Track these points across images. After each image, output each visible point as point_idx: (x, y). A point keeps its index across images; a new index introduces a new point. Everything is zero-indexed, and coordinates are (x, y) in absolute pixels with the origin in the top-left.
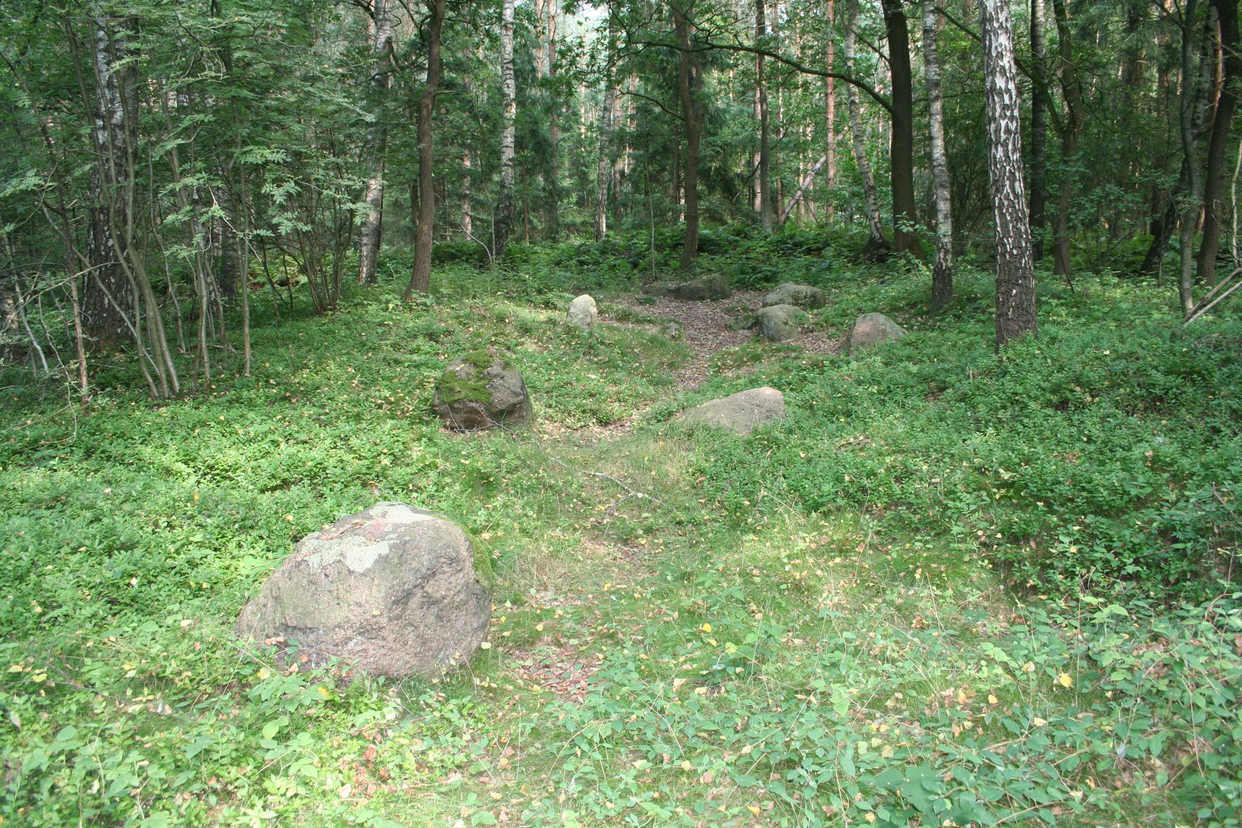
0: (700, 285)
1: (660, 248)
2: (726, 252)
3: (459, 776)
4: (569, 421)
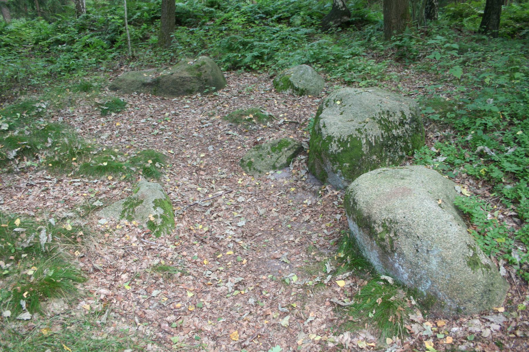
0: (186, 74)
1: (136, 23)
2: (204, 23)
3: (336, 124)
4: (369, 68)
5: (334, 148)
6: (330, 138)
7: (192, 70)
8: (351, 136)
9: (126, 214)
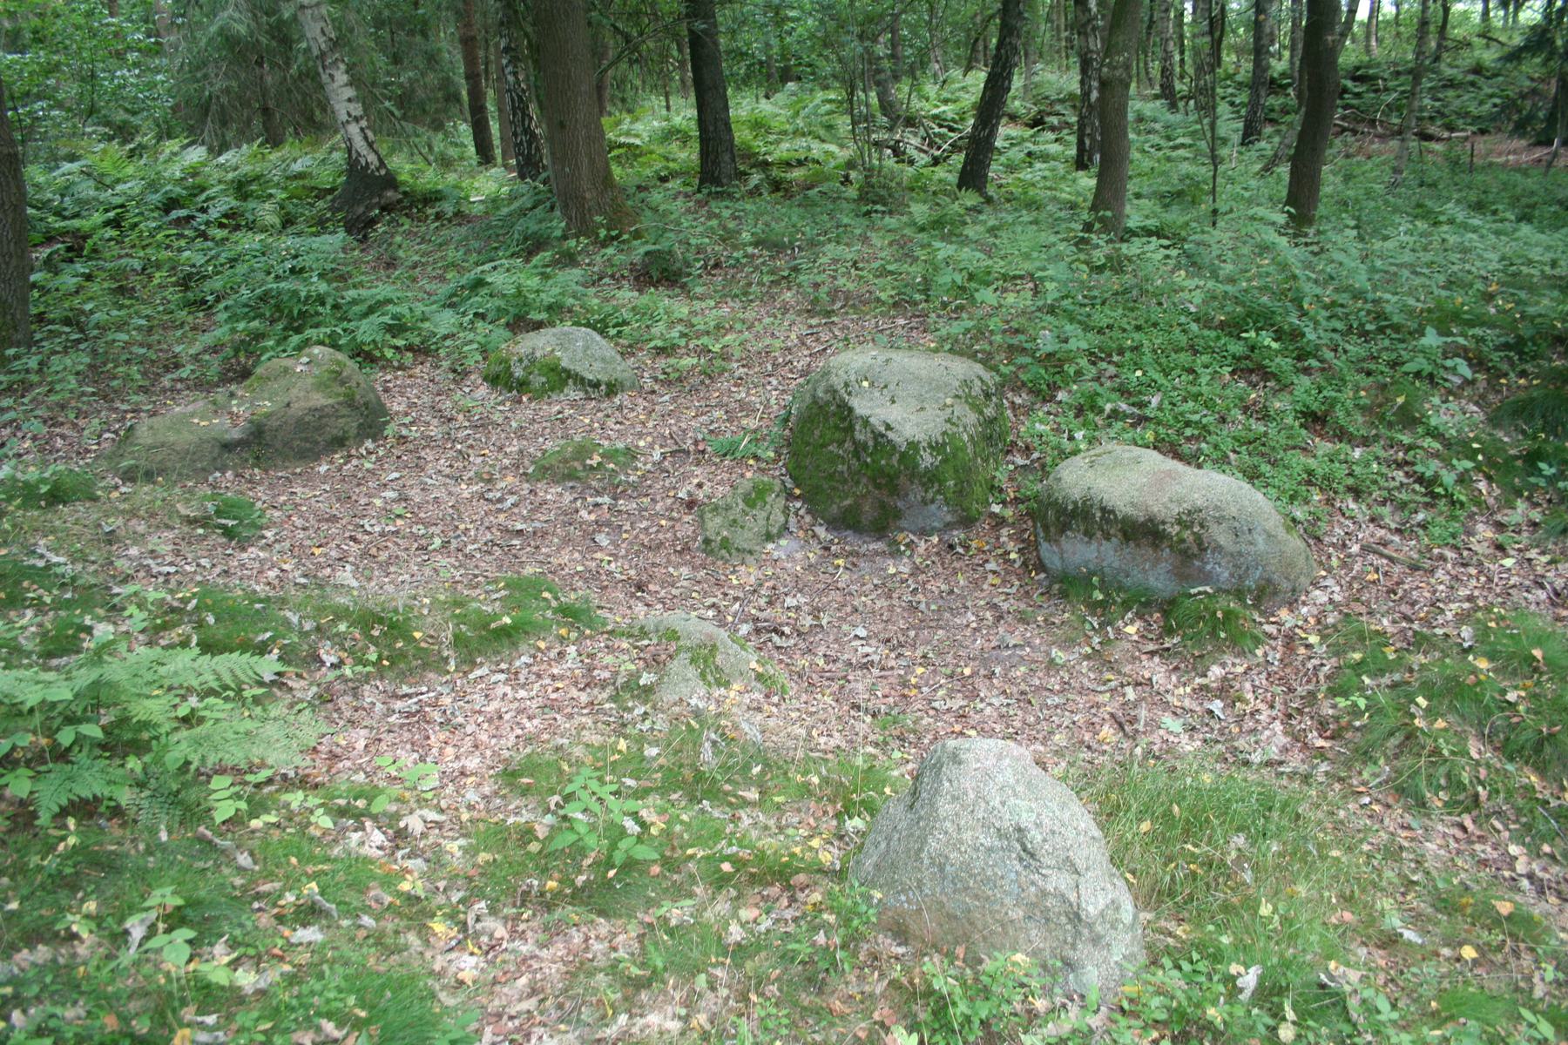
5: (927, 460)
6: (913, 445)
7: (327, 387)
8: (944, 433)
9: (709, 678)
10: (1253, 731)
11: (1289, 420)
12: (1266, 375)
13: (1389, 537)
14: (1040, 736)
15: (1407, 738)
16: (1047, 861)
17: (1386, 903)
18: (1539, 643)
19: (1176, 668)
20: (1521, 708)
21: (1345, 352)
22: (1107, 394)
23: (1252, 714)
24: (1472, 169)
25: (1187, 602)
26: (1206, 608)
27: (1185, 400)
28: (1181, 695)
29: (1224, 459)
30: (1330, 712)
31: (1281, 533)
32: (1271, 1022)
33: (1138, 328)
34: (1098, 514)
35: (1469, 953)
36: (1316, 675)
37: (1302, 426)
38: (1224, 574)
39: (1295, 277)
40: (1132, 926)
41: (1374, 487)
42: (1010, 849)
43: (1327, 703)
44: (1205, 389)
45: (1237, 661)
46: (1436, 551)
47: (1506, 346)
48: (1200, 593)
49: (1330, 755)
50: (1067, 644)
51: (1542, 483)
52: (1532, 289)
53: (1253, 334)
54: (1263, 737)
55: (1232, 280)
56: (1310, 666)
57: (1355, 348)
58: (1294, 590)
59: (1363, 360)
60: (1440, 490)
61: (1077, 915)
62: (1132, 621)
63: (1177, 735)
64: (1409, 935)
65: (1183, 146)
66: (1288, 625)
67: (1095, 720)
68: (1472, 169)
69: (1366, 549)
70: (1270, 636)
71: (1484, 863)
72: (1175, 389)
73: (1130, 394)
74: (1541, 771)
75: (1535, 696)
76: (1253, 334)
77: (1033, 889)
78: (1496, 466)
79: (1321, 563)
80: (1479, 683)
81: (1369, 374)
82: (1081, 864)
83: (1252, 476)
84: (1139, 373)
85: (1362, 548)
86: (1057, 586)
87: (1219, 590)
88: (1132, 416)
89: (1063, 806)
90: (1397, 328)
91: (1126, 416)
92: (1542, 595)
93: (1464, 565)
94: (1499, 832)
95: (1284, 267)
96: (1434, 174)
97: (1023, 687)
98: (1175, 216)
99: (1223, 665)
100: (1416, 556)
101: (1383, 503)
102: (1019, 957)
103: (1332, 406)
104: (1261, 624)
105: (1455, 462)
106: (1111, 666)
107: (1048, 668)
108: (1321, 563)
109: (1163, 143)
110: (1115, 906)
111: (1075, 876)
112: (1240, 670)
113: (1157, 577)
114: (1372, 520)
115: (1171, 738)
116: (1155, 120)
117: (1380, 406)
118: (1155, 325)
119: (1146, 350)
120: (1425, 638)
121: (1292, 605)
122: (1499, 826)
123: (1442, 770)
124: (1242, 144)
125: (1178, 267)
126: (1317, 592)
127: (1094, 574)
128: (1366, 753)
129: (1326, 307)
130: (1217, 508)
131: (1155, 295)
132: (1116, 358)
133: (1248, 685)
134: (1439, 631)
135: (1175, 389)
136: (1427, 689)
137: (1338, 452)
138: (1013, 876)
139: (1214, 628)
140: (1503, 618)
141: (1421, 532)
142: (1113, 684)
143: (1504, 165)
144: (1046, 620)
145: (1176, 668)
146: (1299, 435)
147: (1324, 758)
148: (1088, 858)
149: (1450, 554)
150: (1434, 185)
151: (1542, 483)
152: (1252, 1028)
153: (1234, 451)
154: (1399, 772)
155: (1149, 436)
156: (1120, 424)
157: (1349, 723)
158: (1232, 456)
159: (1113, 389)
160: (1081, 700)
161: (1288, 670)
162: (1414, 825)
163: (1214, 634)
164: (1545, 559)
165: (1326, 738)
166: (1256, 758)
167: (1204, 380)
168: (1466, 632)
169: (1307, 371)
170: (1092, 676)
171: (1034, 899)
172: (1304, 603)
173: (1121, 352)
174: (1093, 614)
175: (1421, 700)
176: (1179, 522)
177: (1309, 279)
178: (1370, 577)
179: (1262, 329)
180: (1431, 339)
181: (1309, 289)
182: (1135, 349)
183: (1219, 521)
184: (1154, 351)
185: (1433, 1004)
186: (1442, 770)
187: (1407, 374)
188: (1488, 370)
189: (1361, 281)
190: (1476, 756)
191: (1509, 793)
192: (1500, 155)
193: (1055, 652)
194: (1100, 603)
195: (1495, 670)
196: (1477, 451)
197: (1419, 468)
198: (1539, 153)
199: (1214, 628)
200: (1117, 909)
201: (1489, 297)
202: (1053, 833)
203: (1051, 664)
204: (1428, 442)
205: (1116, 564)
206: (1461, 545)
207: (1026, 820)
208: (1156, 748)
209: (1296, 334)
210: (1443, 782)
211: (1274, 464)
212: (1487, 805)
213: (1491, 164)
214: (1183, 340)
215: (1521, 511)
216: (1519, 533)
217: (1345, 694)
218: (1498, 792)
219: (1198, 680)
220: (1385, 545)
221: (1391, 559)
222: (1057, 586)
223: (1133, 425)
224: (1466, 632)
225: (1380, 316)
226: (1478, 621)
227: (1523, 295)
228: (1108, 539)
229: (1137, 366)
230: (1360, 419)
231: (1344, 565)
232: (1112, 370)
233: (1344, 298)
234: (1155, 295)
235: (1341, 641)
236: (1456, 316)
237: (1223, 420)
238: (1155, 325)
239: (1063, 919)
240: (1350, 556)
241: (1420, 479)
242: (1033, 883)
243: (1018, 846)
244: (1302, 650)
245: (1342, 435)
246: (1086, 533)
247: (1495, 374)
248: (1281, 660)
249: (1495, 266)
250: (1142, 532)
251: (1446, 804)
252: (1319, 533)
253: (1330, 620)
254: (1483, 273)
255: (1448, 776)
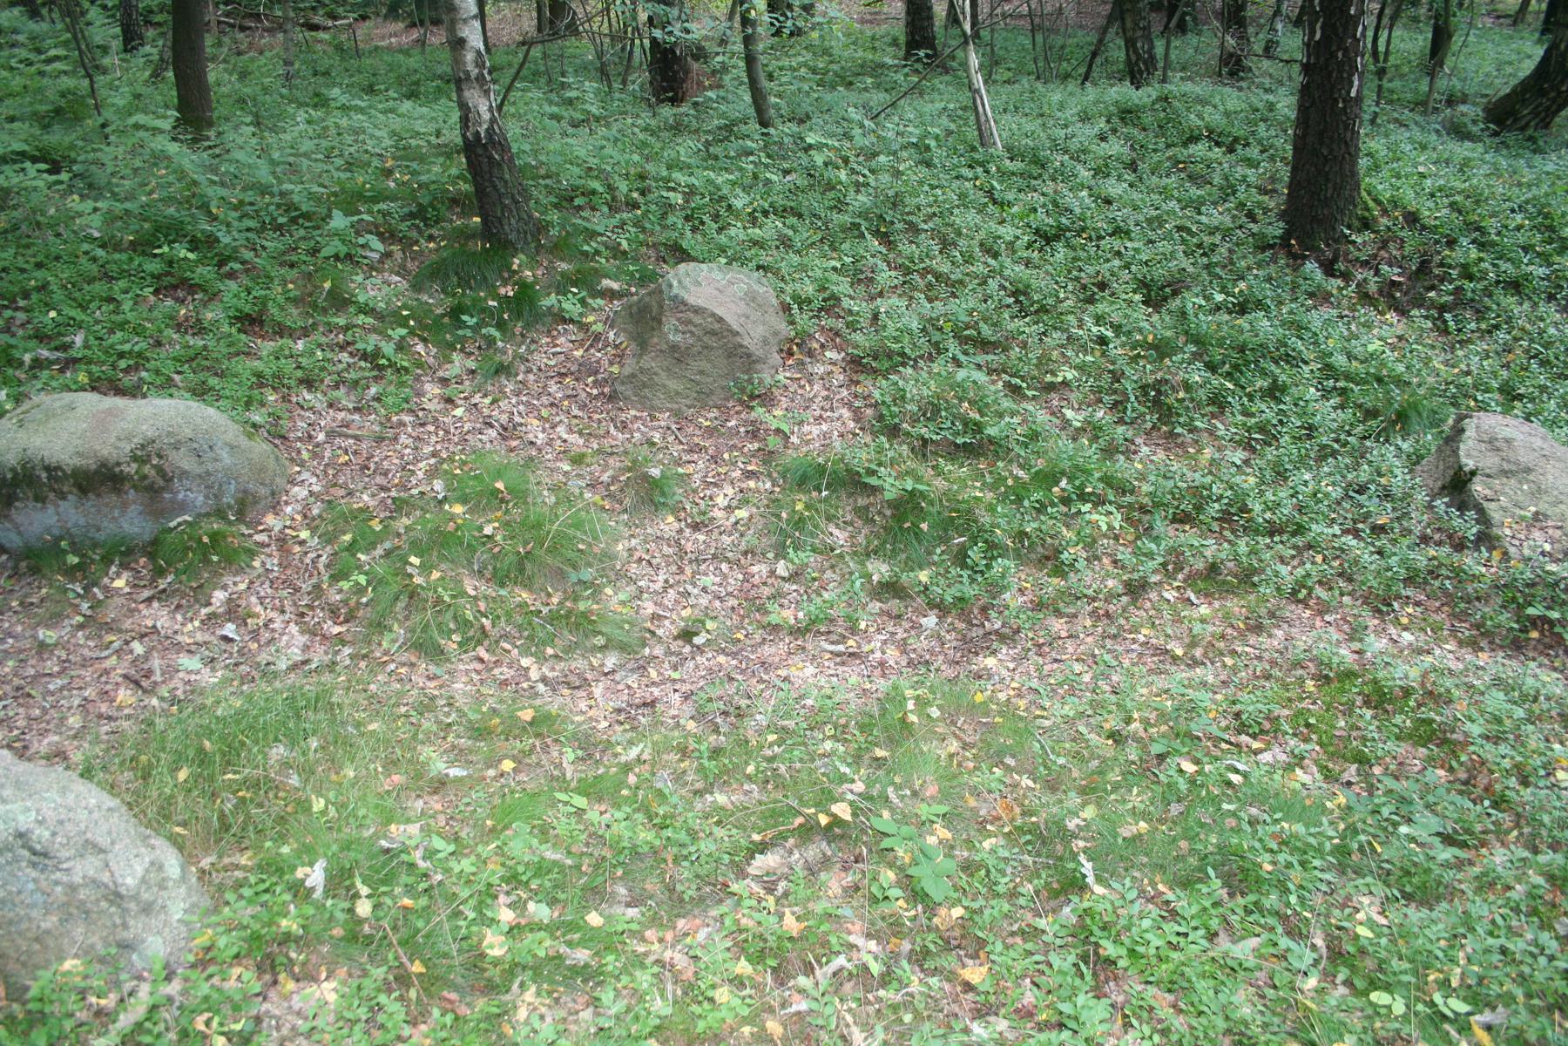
10: (271, 641)
11: (226, 329)
12: (193, 288)
13: (350, 417)
14: (51, 726)
15: (411, 597)
16: (64, 854)
17: (426, 752)
18: (499, 475)
19: (178, 607)
20: (498, 538)
21: (264, 248)
22: (22, 344)
23: (266, 625)
24: (358, 54)
25: (170, 537)
26: (190, 539)
27: (112, 331)
28: (191, 631)
29: (170, 383)
30: (338, 597)
31: (244, 442)
32: (346, 905)
33: (39, 265)
34: (44, 475)
35: (508, 765)
36: (316, 568)
37: (239, 331)
38: (198, 498)
39: (195, 183)
40: (184, 878)
41: (323, 374)
42: (16, 860)
43: (332, 591)
44: (130, 316)
45: (238, 579)
46: (395, 419)
47: (412, 215)
48: (179, 524)
49: (349, 638)
50: (54, 620)
51: (469, 333)
52: (422, 159)
53: (166, 249)
54: (283, 643)
55: (131, 197)
56: (308, 561)
57: (273, 243)
58: (273, 494)
59: (284, 253)
60: (383, 361)
61: (118, 895)
62: (118, 575)
63: (198, 672)
64: (454, 772)
65: (57, 58)
66: (276, 529)
67: (109, 687)
68: (358, 54)
69: (331, 434)
70: (263, 545)
71: (505, 683)
72: (97, 322)
73: (50, 338)
74: (528, 586)
75: (508, 524)
76: (166, 249)
77: (59, 889)
78: (428, 328)
79: (292, 460)
80: (458, 528)
81: (292, 266)
82: (103, 841)
83: (200, 392)
84: (53, 314)
85: (327, 434)
86: (24, 564)
87: (199, 515)
88: (57, 361)
89: (64, 791)
90: (307, 216)
91: (52, 363)
92: (493, 433)
93: (423, 425)
94: (508, 652)
95: (182, 175)
96: (324, 64)
97: (17, 682)
98: (57, 137)
99: (225, 588)
100: (378, 429)
101: (337, 387)
102: (68, 965)
103: (264, 305)
104: (250, 536)
105: (390, 332)
106: (110, 628)
107: (39, 653)
108: (292, 460)
109: (32, 56)
110: (157, 866)
111: (101, 856)
112: (242, 586)
113: (132, 522)
114: (331, 405)
115: (193, 677)
116: (15, 31)
117: (310, 295)
118: (57, 258)
119: (54, 287)
120: (405, 502)
121: (275, 508)
122: (507, 646)
123: (449, 615)
124: (126, 51)
125: (70, 189)
126: (296, 489)
127: (61, 538)
128: (379, 624)
129: (235, 208)
130: (169, 434)
131: (51, 226)
132: (22, 303)
133: (254, 599)
134: (415, 492)
135: (97, 322)
136: (416, 547)
137: (282, 349)
138: (31, 886)
139: (205, 555)
140: (464, 463)
141: (376, 404)
142: (116, 645)
143: (389, 48)
144: (22, 604)
145: (178, 607)
146: (239, 340)
147: (344, 643)
148: (109, 833)
149: (407, 418)
150: (327, 73)
151: (469, 333)
152: (332, 918)
153: (179, 373)
154: (413, 631)
155: (82, 378)
156: (46, 373)
157: (358, 603)
158: (177, 378)
159: (30, 337)
160: (87, 674)
161: (289, 572)
162: (439, 672)
163: (206, 560)
164: (487, 401)
165: (341, 624)
166: (282, 665)
167: (127, 306)
168: (438, 485)
169: (231, 275)
170: (92, 644)
171: (65, 899)
172: (286, 503)
173: (26, 296)
174: (73, 581)
175: (413, 559)
176: (135, 459)
177: (214, 182)
178: (341, 460)
179: (174, 242)
180: (339, 221)
181: (214, 192)
182: (43, 288)
183: (176, 446)
184: (64, 287)
185: (489, 822)
186: (449, 615)
187: (328, 258)
188: (400, 240)
189: (264, 174)
190: (473, 593)
191: (509, 615)
192: (383, 38)
193: (42, 633)
194: (80, 567)
195: (470, 511)
196: (407, 318)
197: (360, 346)
198: (415, 34)
199: (205, 555)
200: (161, 868)
201: (388, 173)
202: (61, 822)
203: (42, 647)
204: (361, 319)
205: (82, 521)
206: (414, 407)
207: (25, 821)
208: (179, 693)
209: (211, 241)
210: (452, 626)
211: (221, 375)
212: (494, 633)
213: (377, 48)
214: (94, 268)
215: (458, 364)
216: (461, 383)
217: (344, 575)
218: (498, 617)
219: (204, 611)
220: (347, 427)
221: (356, 437)
222: (24, 564)
223: (62, 371)
224: (438, 485)
225: (291, 207)
226: (446, 472)
227: (414, 165)
228: (64, 498)
229: (49, 306)
230: (295, 312)
231: (315, 455)
232: (21, 316)
233: (249, 196)
234: (51, 226)
235: (330, 528)
236: (359, 196)
237: (159, 344)
238: (57, 258)
239: (104, 904)
240: (318, 445)
241: (365, 356)
242: (57, 883)
243: (26, 853)
244: (297, 549)
245: (281, 331)
246: (37, 499)
247: (407, 243)
248: (280, 565)
249: (387, 142)
250: (99, 480)
251: (460, 644)
252: (283, 432)
253: (315, 512)
254: (378, 150)
255: (455, 618)
